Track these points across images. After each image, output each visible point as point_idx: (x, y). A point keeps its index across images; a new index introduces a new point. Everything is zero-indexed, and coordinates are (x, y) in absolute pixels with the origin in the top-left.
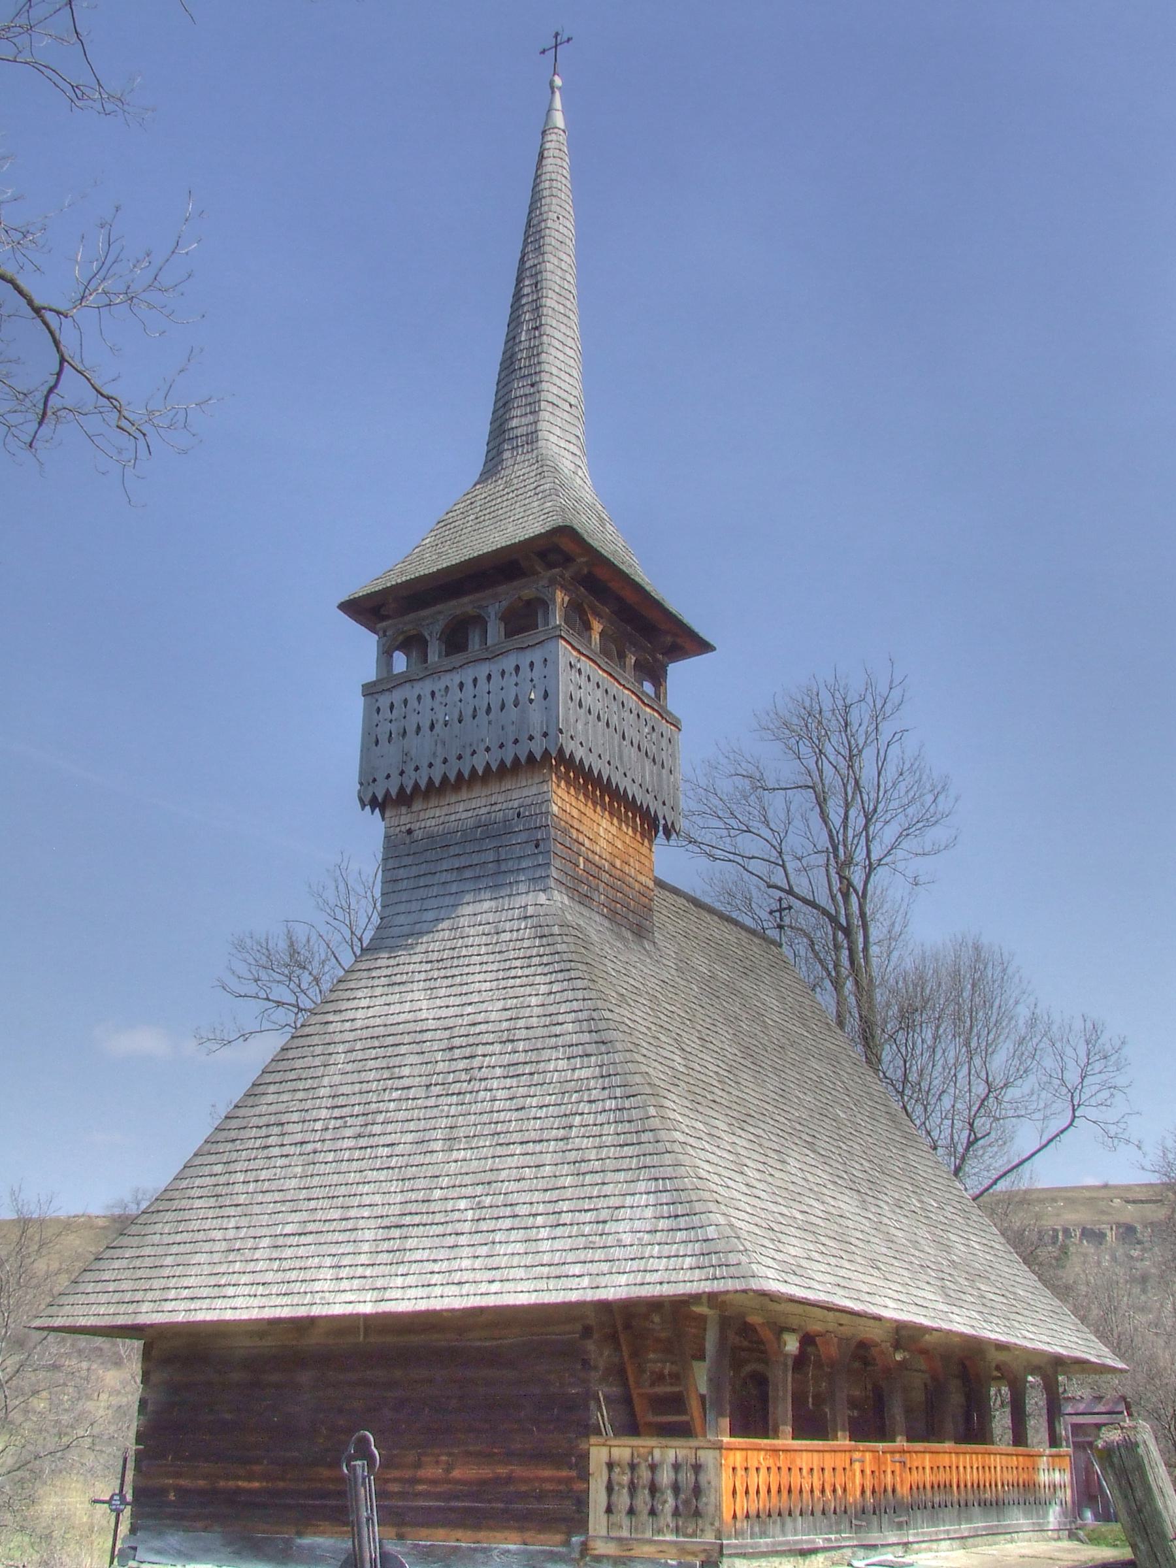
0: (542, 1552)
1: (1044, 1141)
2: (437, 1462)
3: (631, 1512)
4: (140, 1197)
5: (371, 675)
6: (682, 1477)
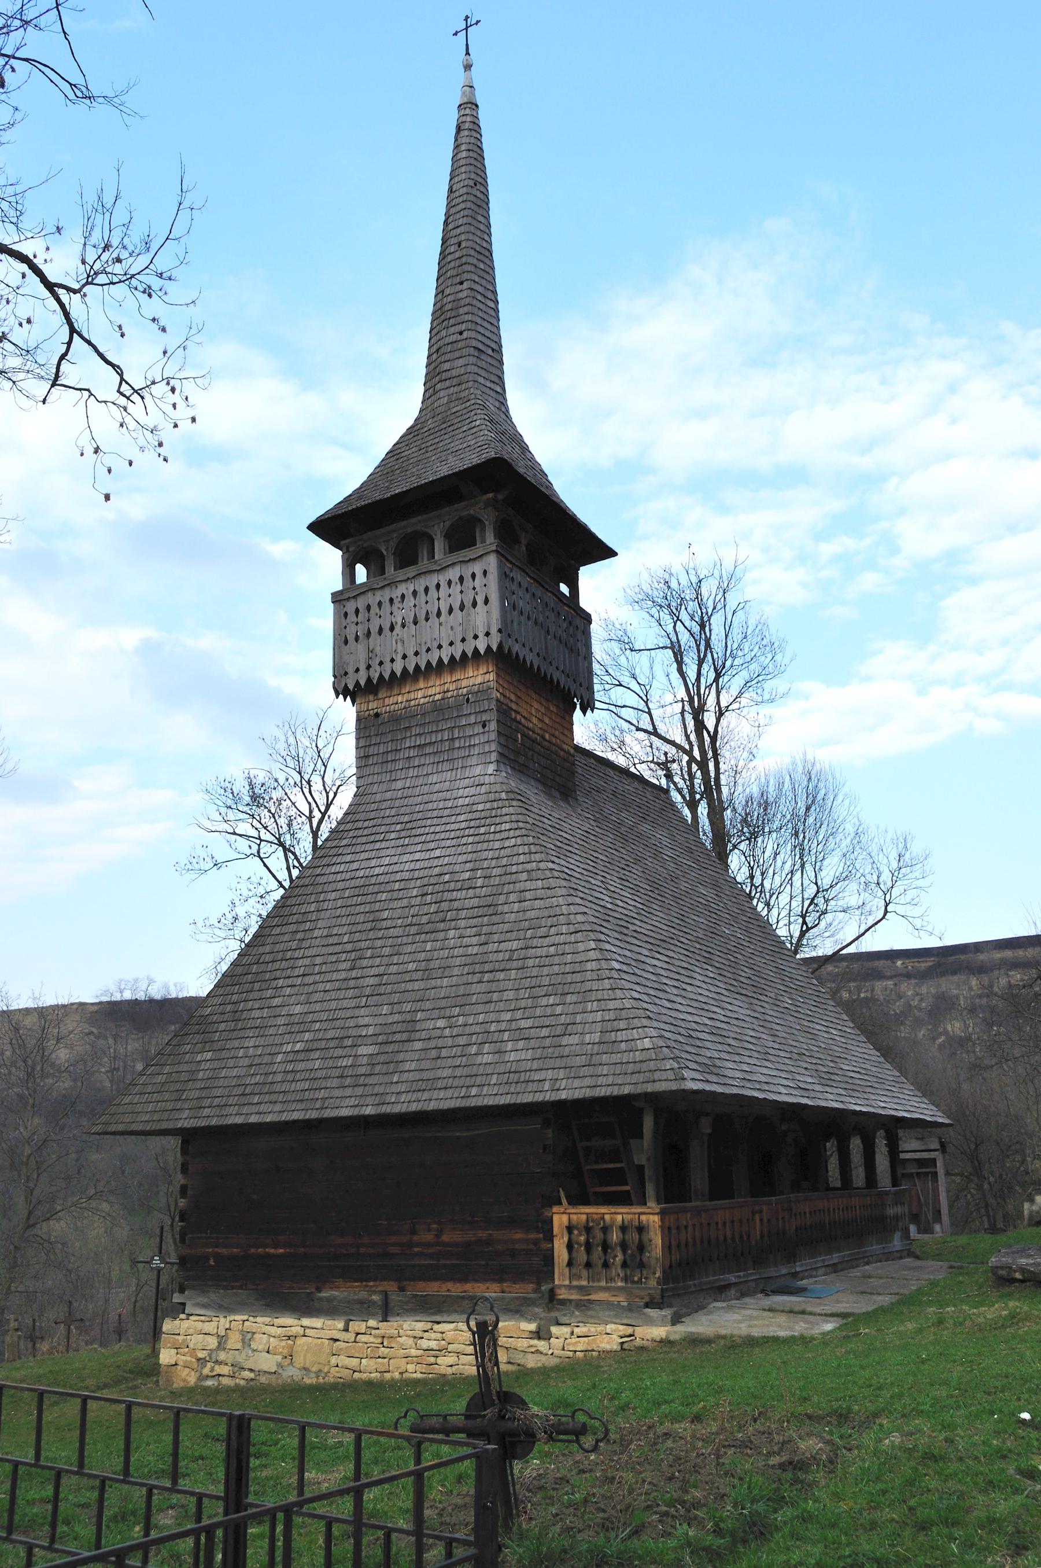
0: (518, 1298)
1: (862, 930)
2: (429, 1230)
3: (588, 1265)
4: (122, 987)
5: (339, 587)
6: (628, 1237)
